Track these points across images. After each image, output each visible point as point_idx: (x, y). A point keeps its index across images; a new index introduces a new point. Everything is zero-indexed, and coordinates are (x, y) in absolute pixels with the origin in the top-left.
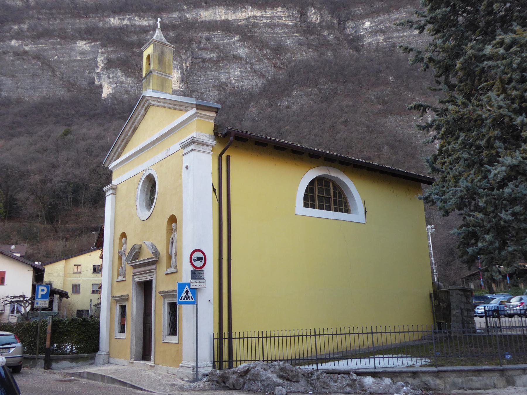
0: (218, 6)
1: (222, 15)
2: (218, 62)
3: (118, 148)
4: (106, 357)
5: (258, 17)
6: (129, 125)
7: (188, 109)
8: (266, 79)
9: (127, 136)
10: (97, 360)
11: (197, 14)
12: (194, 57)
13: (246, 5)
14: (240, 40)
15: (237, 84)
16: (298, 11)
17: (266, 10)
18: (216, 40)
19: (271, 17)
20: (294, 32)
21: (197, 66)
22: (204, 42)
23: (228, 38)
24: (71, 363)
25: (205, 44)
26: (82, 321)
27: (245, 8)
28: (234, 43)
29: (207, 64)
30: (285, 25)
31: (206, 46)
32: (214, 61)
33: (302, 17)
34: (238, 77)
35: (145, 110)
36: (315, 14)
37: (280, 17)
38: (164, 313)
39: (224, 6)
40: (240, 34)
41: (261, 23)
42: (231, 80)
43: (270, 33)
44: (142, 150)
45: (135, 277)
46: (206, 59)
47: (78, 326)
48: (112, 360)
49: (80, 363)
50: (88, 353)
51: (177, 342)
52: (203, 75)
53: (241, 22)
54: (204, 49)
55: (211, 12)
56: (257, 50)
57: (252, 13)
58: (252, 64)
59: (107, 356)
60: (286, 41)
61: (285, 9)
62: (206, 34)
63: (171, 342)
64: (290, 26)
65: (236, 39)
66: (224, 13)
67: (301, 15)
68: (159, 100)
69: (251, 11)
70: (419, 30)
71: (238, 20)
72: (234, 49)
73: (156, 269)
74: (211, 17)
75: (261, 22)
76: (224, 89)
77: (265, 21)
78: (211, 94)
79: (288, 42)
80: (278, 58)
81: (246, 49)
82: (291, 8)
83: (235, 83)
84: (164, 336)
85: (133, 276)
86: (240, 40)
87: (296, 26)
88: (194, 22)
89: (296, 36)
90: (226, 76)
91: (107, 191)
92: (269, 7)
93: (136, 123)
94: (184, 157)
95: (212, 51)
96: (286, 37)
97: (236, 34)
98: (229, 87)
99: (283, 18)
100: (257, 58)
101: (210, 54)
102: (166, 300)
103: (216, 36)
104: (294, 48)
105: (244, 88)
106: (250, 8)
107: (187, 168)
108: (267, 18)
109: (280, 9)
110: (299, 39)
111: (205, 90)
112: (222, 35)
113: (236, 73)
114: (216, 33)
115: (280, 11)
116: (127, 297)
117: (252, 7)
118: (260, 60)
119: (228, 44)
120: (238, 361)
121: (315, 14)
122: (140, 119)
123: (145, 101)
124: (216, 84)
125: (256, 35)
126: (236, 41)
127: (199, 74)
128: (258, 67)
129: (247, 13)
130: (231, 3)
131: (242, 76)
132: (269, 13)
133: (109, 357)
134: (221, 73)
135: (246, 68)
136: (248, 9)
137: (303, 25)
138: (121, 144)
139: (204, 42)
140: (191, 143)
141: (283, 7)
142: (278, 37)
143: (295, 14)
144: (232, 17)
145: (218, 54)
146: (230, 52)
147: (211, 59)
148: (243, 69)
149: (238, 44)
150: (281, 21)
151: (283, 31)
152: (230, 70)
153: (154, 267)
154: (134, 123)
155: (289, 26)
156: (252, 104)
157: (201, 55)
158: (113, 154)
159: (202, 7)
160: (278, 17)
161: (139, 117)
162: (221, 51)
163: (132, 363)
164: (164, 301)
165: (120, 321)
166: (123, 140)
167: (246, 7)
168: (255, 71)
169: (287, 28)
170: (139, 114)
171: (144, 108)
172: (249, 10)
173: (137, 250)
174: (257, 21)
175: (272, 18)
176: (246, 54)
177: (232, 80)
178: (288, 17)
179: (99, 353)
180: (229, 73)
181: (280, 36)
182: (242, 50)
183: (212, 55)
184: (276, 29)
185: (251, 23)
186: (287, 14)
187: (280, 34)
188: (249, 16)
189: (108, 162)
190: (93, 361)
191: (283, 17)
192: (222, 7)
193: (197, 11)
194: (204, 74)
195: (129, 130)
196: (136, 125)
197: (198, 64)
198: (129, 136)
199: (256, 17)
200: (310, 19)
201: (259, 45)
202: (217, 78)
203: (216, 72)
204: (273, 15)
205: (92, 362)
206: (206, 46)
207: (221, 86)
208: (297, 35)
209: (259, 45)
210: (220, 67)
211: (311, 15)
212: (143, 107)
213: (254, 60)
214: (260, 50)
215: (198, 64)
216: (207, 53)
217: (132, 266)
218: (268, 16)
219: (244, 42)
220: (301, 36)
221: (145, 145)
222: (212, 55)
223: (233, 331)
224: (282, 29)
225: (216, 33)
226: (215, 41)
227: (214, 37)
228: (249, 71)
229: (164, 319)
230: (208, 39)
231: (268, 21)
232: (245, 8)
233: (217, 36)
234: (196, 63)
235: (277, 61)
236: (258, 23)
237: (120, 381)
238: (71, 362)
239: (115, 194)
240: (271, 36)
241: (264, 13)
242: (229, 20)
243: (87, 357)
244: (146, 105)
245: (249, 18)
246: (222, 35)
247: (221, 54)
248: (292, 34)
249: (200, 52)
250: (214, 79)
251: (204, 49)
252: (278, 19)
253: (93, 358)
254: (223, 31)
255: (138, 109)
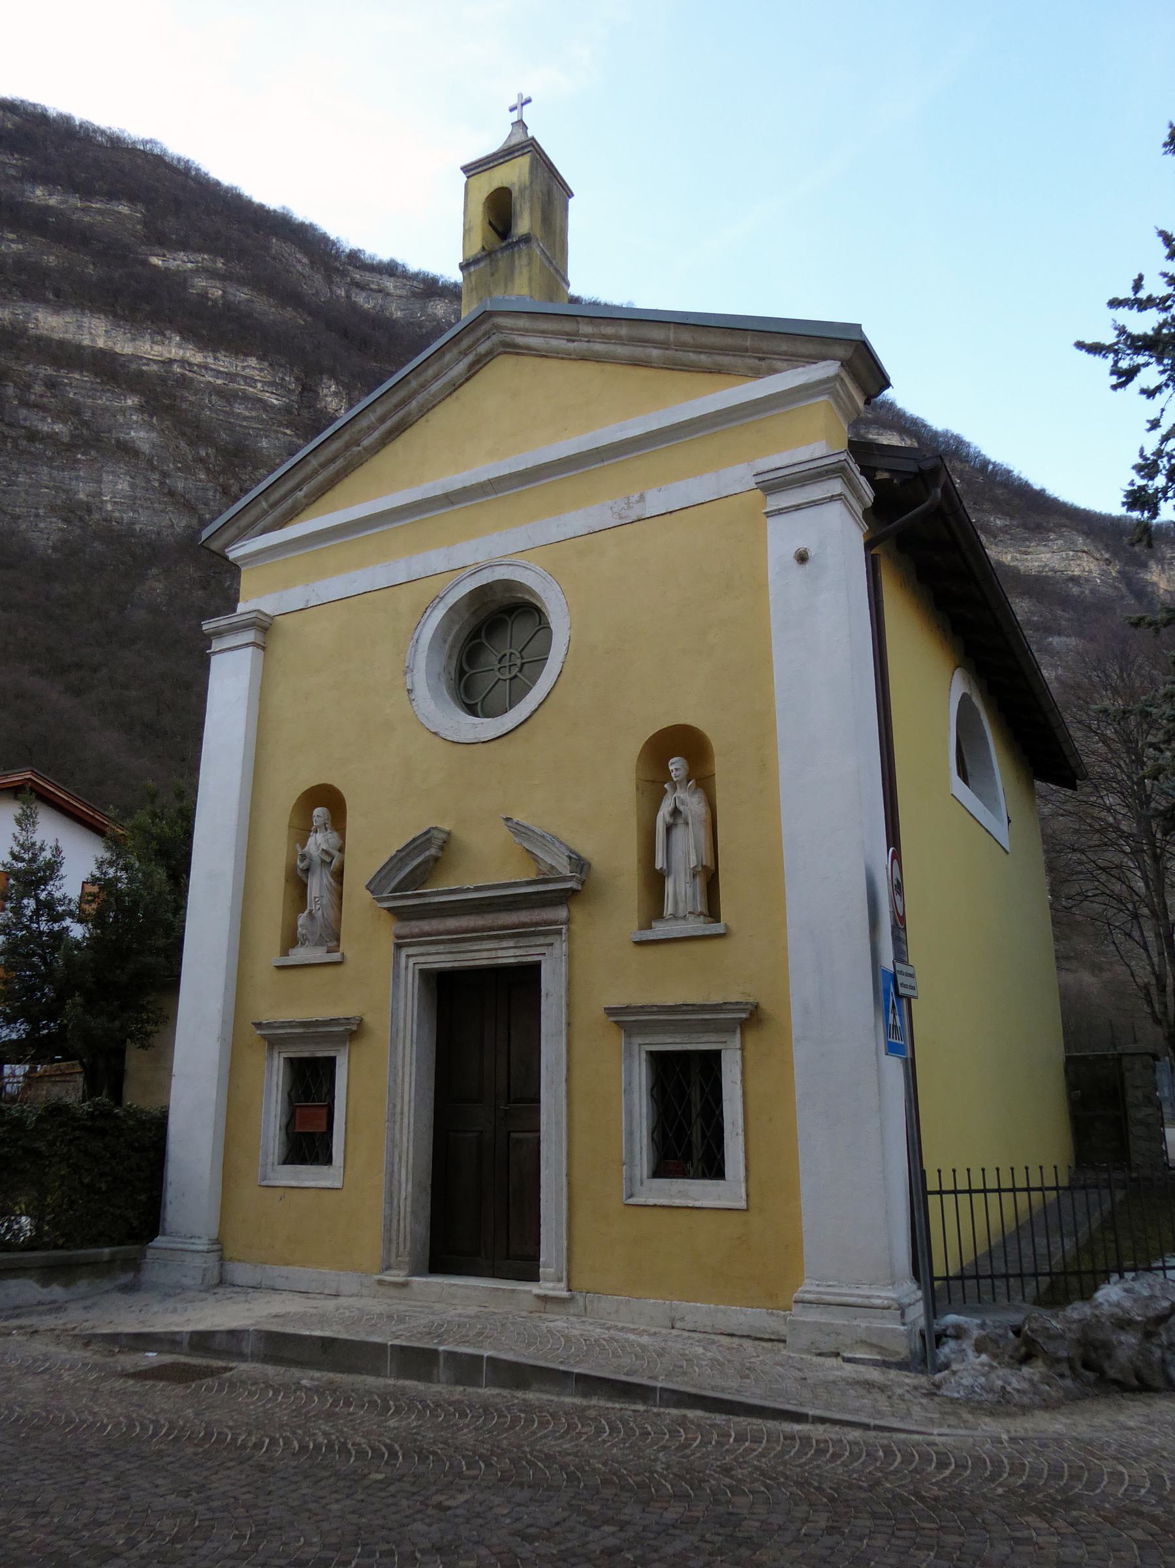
0: (91, 311)
1: (99, 336)
2: (72, 447)
3: (298, 487)
4: (212, 1260)
5: (196, 365)
6: (380, 410)
7: (779, 364)
8: (199, 518)
9: (356, 449)
10: (152, 1272)
11: (28, 314)
12: (6, 419)
13: (167, 329)
14: (140, 409)
15: (117, 514)
16: (297, 379)
17: (218, 355)
18: (75, 394)
19: (227, 374)
20: (280, 424)
21: (9, 445)
22: (38, 388)
23: (109, 394)
24: (43, 1286)
25: (42, 396)
26: (91, 1115)
27: (164, 335)
28: (123, 411)
29: (41, 446)
30: (260, 400)
31: (45, 400)
32: (63, 443)
33: (306, 394)
34: (124, 497)
35: (472, 365)
36: (335, 394)
37: (248, 380)
38: (628, 1091)
39: (106, 316)
40: (141, 393)
41: (201, 382)
42: (102, 502)
43: (221, 410)
44: (449, 499)
45: (404, 952)
46: (38, 432)
47: (77, 1133)
48: (241, 1273)
49: (82, 1286)
50: (111, 1242)
51: (742, 1204)
52: (25, 470)
53: (148, 365)
54: (36, 406)
55: (68, 319)
56: (183, 444)
57: (181, 352)
58: (165, 475)
59: (213, 1257)
60: (259, 439)
61: (266, 364)
62: (47, 370)
63: (691, 1203)
64: (273, 406)
65: (130, 402)
66: (106, 331)
67: (303, 389)
68: (586, 329)
69: (179, 346)
70: (1119, 378)
71: (141, 358)
72: (121, 425)
73: (568, 922)
74: (66, 332)
75: (202, 379)
76: (81, 519)
77: (211, 379)
78: (42, 525)
79: (264, 443)
80: (236, 476)
81: (154, 435)
82: (281, 366)
83: (113, 511)
84: (631, 1179)
85: (399, 947)
86: (140, 409)
87: (287, 410)
88: (16, 332)
89: (285, 434)
90: (91, 487)
91: (219, 634)
92: (226, 350)
93: (414, 404)
94: (772, 523)
95: (59, 417)
96: (259, 429)
97: (133, 391)
98: (96, 516)
99: (259, 385)
100: (180, 462)
101: (54, 422)
102: (637, 1040)
103: (74, 384)
104: (278, 461)
105: (138, 527)
106: (178, 338)
107: (802, 558)
108: (218, 373)
109: (253, 361)
110: (291, 443)
111: (24, 510)
112: (92, 383)
113: (120, 487)
114: (77, 376)
115: (252, 366)
116: (354, 1028)
117: (183, 338)
118: (187, 469)
119: (105, 409)
120: (971, 1277)
121: (335, 394)
122: (434, 396)
123: (484, 334)
124: (59, 502)
125: (184, 406)
126: (130, 408)
127: (14, 465)
128: (180, 485)
129: (166, 348)
130: (127, 312)
131: (136, 498)
132: (225, 363)
133: (222, 1258)
134: (77, 478)
135: (148, 481)
136: (170, 339)
137: (305, 413)
138: (315, 473)
139: (38, 388)
140: (834, 471)
141: (261, 359)
142: (240, 426)
143: (290, 383)
144: (123, 346)
145: (76, 428)
146: (110, 431)
147: (52, 438)
148: (140, 482)
149: (134, 418)
150: (251, 389)
151: (254, 414)
152: (104, 475)
153: (561, 913)
154: (404, 402)
155: (270, 407)
156: (154, 571)
157: (25, 419)
158: (264, 505)
159: (44, 301)
160: (245, 378)
161: (435, 387)
162: (85, 424)
163: (405, 1285)
164: (629, 1045)
165: (285, 1121)
166: (332, 460)
167: (168, 333)
168: (171, 493)
169: (265, 410)
170: (436, 377)
171: (470, 358)
172: (173, 343)
173: (433, 851)
174: (190, 374)
175: (232, 377)
176: (154, 446)
177: (106, 501)
178: (271, 384)
179: (160, 1241)
180: (99, 481)
181: (245, 423)
182: (142, 434)
183: (58, 427)
184: (237, 406)
185: (174, 374)
186: (269, 378)
187: (245, 418)
188: (172, 356)
189: (232, 531)
190: (131, 1275)
191: (260, 381)
192: (102, 317)
193: (28, 306)
194: (29, 468)
195: (371, 428)
196: (409, 414)
197: (15, 440)
198: (366, 449)
199: (190, 364)
200: (323, 403)
201: (188, 431)
202: (64, 487)
203: (63, 470)
204: (233, 370)
205: (126, 1278)
206: (45, 400)
207: (72, 511)
208: (288, 432)
209: (188, 431)
210: (77, 461)
211: (326, 396)
212: (465, 354)
213: (171, 466)
214: (191, 444)
215: (15, 440)
216: (43, 419)
217: (389, 909)
218: (222, 369)
219: (152, 417)
220: (298, 438)
221: (484, 478)
222: (58, 427)
223: (930, 1165)
224: (251, 409)
225: (77, 376)
226: (71, 395)
227: (70, 385)
228: (154, 488)
229: (630, 1113)
230: (52, 384)
231: (219, 382)
232: (164, 335)
233: (77, 384)
234: (7, 437)
235: (231, 482)
236: (192, 379)
237: (582, 1378)
238: (45, 1283)
239: (264, 648)
240: (221, 418)
241: (210, 360)
242: (116, 353)
243: (111, 1261)
244: (483, 348)
245: (171, 361)
246: (92, 383)
247: (85, 432)
248: (275, 427)
249: (23, 412)
250: (56, 488)
251: (36, 406)
252: (246, 384)
253: (134, 1264)
254: (96, 375)
255: (444, 355)
